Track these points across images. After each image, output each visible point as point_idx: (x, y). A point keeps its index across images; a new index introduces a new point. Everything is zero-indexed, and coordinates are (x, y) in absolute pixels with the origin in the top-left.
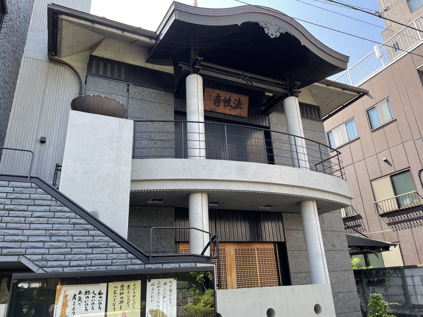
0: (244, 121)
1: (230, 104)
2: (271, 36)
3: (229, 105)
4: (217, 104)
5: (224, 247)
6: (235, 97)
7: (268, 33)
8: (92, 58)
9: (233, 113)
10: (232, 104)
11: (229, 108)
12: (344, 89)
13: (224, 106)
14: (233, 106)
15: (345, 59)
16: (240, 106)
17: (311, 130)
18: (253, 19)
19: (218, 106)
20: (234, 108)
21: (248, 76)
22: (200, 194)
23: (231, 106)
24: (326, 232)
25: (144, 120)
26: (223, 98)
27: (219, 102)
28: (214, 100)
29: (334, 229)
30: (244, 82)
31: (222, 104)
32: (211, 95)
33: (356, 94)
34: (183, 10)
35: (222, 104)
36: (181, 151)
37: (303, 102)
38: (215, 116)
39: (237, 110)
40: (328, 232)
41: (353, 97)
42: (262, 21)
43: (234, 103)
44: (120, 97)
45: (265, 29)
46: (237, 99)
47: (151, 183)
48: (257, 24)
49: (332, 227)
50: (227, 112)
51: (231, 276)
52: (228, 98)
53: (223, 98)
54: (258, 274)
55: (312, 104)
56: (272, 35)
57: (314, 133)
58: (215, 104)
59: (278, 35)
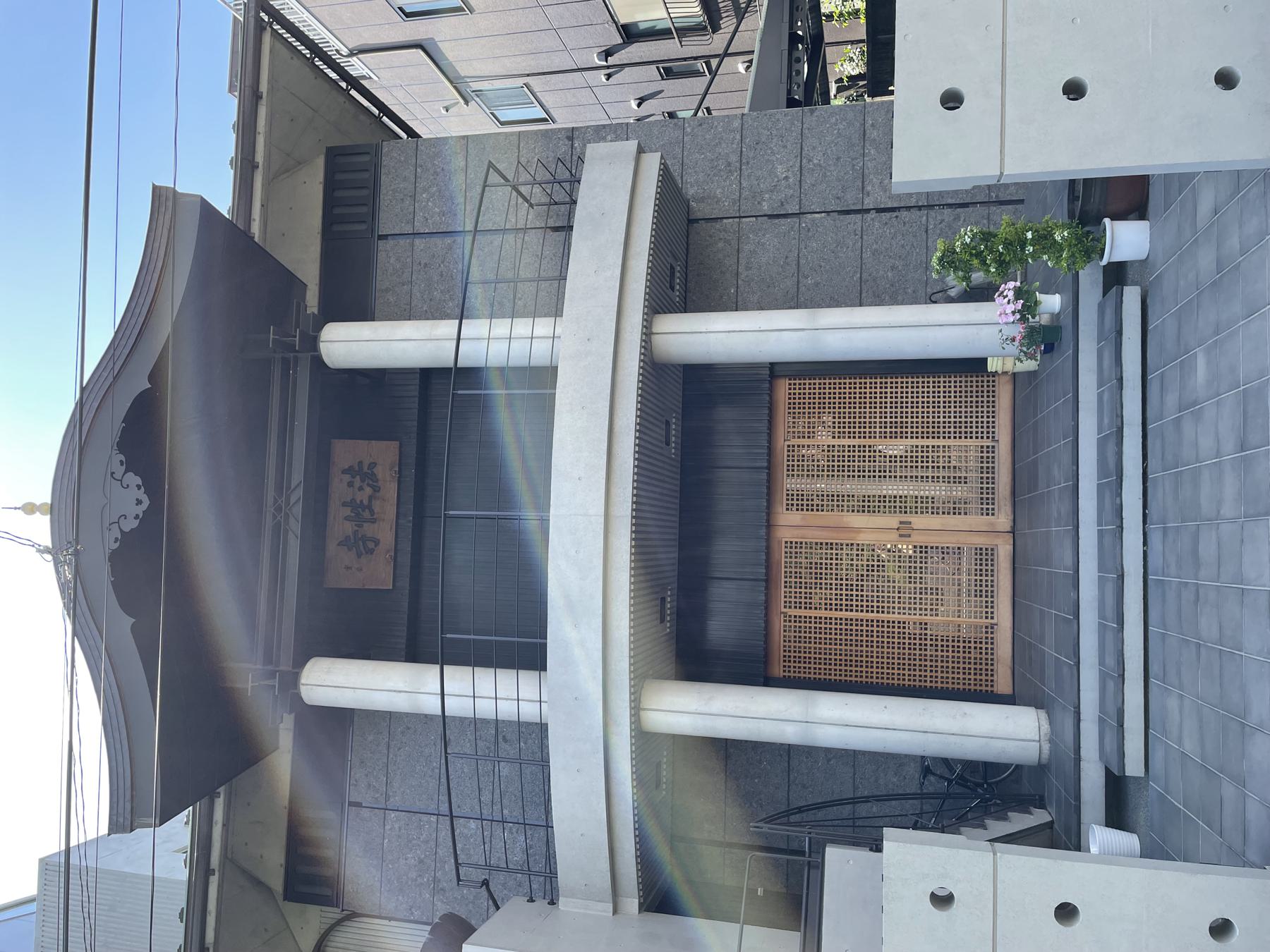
0: (412, 450)
1: (366, 502)
2: (146, 503)
3: (369, 507)
4: (371, 545)
5: (780, 542)
6: (339, 487)
7: (137, 517)
8: (292, 894)
9: (390, 490)
10: (364, 496)
11: (377, 506)
12: (257, 96)
13: (373, 521)
14: (368, 491)
15: (163, 199)
16: (365, 469)
17: (414, 197)
18: (102, 576)
19: (377, 542)
20: (376, 490)
21: (276, 501)
22: (642, 713)
23: (370, 498)
24: (745, 193)
25: (444, 767)
26: (349, 528)
27: (364, 539)
28: (359, 555)
29: (734, 158)
30: (298, 510)
31: (368, 529)
32: (348, 568)
33: (267, 38)
34: (128, 806)
35: (368, 529)
36: (526, 746)
37: (320, 213)
38: (407, 547)
39: (380, 476)
40: (744, 184)
41: (278, 45)
42: (102, 544)
43: (361, 489)
44: (388, 827)
45: (127, 529)
46: (347, 478)
47: (615, 789)
48: (114, 557)
49: (729, 164)
50: (391, 511)
51: (858, 530)
52: (347, 511)
53: (349, 528)
54: (856, 442)
55: (320, 176)
56: (139, 502)
57: (425, 190)
58: (371, 552)
59: (133, 479)
